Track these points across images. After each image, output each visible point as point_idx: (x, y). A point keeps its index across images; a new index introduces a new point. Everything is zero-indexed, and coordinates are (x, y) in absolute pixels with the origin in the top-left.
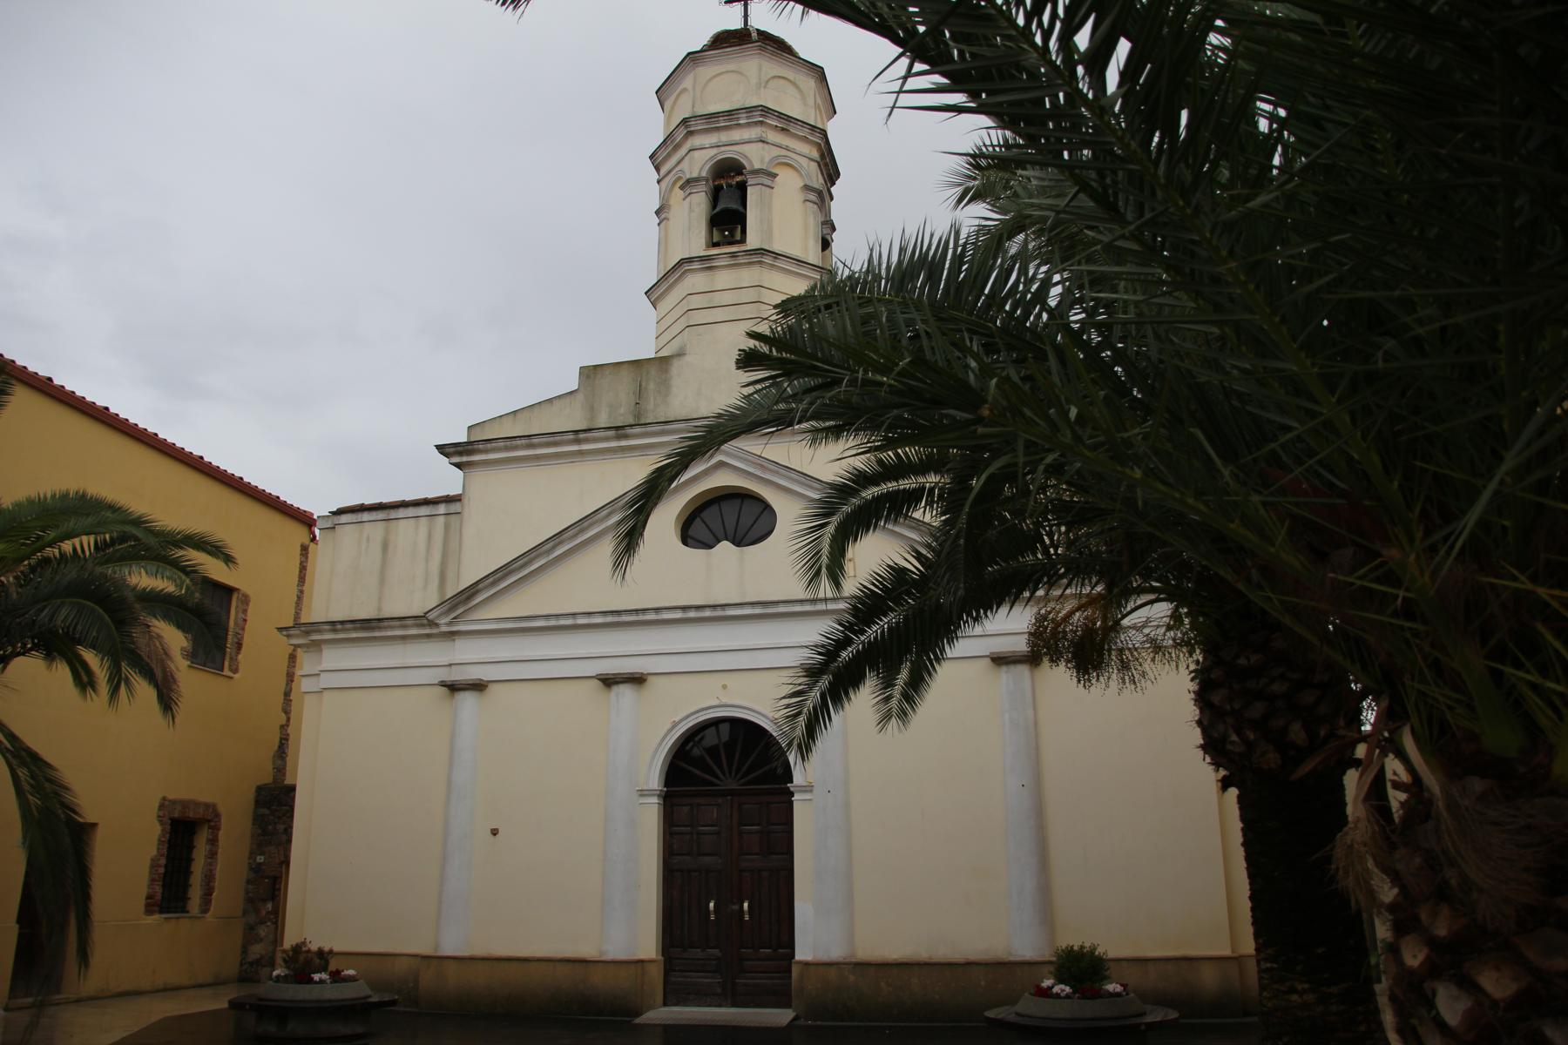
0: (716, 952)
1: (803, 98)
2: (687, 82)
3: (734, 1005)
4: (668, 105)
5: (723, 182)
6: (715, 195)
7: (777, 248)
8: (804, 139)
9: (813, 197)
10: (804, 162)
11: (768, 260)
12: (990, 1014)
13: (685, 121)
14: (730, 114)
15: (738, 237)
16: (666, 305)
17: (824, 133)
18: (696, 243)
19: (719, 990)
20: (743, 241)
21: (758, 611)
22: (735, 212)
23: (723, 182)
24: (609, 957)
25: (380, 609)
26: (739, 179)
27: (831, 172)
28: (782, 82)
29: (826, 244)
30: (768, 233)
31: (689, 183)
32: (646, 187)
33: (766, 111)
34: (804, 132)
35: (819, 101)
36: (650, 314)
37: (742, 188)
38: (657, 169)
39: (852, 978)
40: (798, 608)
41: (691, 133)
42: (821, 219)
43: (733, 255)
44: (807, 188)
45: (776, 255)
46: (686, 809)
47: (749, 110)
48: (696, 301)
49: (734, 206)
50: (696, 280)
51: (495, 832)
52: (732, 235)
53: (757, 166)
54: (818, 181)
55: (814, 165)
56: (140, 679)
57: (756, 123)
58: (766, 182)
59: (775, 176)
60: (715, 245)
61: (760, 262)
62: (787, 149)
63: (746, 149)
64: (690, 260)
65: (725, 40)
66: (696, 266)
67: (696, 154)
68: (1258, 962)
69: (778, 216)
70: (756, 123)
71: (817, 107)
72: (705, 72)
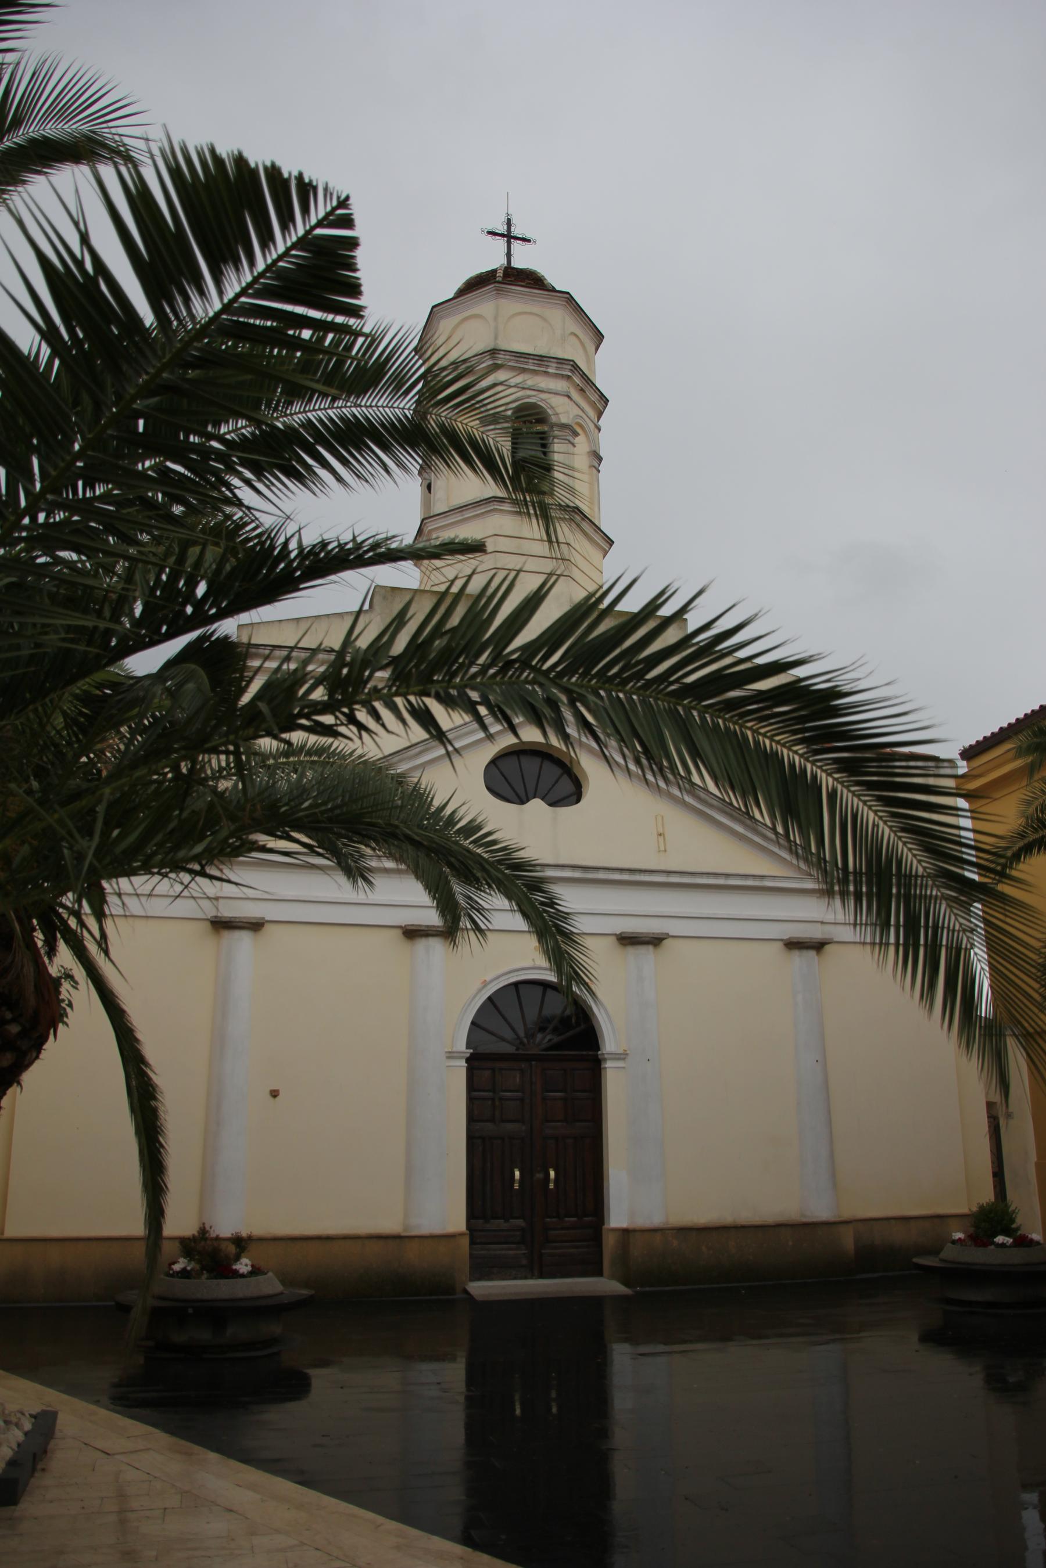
0: (520, 1222)
3: (542, 1276)
12: (915, 1260)
14: (541, 359)
19: (524, 1262)
21: (577, 874)
24: (425, 1231)
34: (594, 397)
39: (675, 1243)
40: (617, 876)
46: (487, 1073)
47: (561, 361)
51: (274, 1094)
53: (564, 420)
68: (472, 1243)
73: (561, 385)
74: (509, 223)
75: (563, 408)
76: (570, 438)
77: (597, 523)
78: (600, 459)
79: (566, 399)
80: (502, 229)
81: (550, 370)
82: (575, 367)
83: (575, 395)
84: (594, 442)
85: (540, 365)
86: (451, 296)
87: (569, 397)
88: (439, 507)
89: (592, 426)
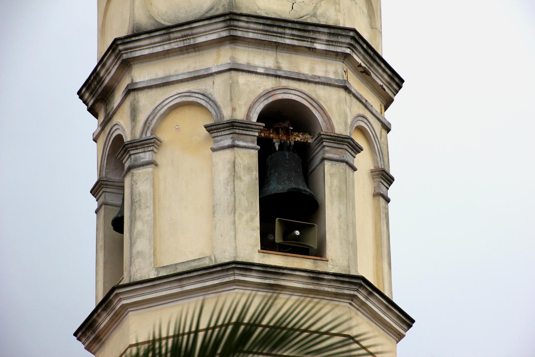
41: (233, 40)
47: (335, 31)
53: (340, 129)
57: (337, 55)
61: (352, 297)
63: (322, 93)
73: (332, 69)
75: (337, 111)
76: (348, 157)
77: (387, 294)
78: (389, 180)
79: (342, 93)
81: (318, 46)
82: (357, 39)
83: (356, 84)
84: (380, 153)
85: (301, 38)
87: (347, 89)
88: (141, 268)
89: (377, 126)
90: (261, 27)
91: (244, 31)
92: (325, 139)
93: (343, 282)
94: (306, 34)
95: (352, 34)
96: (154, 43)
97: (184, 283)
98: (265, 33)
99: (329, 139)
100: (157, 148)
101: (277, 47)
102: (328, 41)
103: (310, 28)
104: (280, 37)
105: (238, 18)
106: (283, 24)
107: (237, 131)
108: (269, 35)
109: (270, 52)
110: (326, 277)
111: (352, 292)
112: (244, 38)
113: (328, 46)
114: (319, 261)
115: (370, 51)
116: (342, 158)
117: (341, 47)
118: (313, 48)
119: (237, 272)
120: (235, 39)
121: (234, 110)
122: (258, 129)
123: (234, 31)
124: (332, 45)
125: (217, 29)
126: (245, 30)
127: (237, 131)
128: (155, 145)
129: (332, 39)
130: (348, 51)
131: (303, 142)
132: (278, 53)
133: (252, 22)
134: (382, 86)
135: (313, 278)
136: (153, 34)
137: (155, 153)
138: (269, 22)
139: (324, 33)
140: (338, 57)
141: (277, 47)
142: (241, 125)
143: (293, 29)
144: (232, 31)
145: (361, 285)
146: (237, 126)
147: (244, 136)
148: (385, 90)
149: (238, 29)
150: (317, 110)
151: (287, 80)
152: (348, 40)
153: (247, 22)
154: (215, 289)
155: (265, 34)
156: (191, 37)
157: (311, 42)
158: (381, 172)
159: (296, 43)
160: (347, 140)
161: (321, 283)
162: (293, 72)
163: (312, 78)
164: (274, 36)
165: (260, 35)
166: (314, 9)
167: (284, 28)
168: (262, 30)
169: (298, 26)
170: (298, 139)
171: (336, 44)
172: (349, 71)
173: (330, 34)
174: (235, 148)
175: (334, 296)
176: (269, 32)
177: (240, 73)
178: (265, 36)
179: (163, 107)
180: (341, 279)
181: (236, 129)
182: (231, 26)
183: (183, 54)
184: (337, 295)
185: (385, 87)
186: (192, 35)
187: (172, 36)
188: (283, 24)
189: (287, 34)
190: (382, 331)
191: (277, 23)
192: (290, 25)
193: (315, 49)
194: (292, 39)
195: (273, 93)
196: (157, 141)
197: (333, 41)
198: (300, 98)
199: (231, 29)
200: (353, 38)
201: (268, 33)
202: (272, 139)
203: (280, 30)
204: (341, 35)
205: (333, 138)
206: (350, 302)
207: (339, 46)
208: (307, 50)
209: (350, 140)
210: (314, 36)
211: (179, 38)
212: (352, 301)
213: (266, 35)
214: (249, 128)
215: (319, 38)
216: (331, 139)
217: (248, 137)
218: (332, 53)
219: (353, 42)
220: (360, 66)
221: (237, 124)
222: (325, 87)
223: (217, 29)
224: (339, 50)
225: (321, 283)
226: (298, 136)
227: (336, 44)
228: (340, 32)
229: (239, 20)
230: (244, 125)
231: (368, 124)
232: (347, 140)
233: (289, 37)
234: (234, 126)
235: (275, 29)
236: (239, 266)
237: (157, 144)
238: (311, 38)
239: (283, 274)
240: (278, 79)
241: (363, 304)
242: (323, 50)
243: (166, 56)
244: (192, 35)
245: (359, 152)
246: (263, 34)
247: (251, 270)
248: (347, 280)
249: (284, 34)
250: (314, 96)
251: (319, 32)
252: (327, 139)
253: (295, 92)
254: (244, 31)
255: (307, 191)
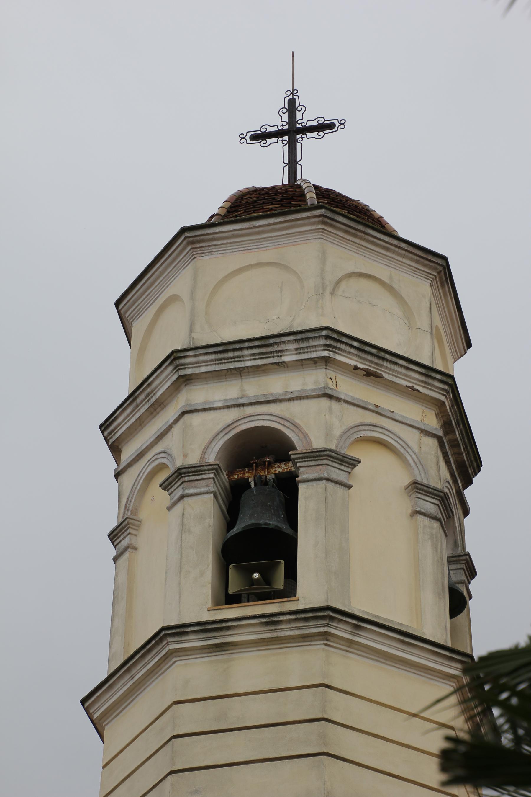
1: (408, 313)
2: (180, 282)
4: (139, 327)
5: (250, 476)
6: (233, 501)
7: (358, 607)
8: (411, 393)
9: (430, 506)
10: (411, 437)
11: (341, 631)
13: (174, 357)
14: (264, 343)
15: (280, 583)
16: (122, 728)
17: (449, 382)
18: (197, 602)
20: (290, 590)
22: (276, 532)
23: (250, 476)
25: (327, 601)
26: (281, 468)
27: (463, 457)
28: (364, 283)
29: (458, 603)
30: (340, 574)
31: (181, 476)
32: (94, 487)
33: (335, 338)
35: (438, 321)
36: (94, 748)
37: (288, 487)
38: (115, 449)
41: (186, 380)
42: (446, 552)
43: (270, 620)
44: (418, 488)
45: (359, 622)
47: (302, 336)
48: (191, 718)
49: (273, 521)
50: (191, 673)
52: (267, 579)
53: (318, 443)
54: (439, 475)
55: (431, 444)
56: (439, 487)
57: (315, 361)
58: (341, 476)
59: (352, 463)
60: (231, 599)
61: (325, 636)
62: (377, 411)
63: (295, 410)
64: (179, 630)
65: (249, 207)
66: (192, 642)
67: (195, 420)
69: (358, 542)
70: (315, 361)
71: (435, 334)
72: (214, 265)
73: (313, 379)
74: (260, 137)
79: (325, 402)
80: (278, 149)
85: (264, 355)
86: (203, 220)
90: (213, 357)
91: (194, 367)
92: (297, 459)
93: (306, 619)
94: (269, 349)
95: (324, 333)
96: (128, 416)
97: (133, 672)
98: (220, 362)
99: (302, 458)
100: (137, 530)
101: (240, 374)
102: (297, 349)
103: (272, 341)
104: (238, 361)
105: (182, 354)
106: (238, 346)
107: (187, 479)
108: (225, 363)
109: (234, 382)
110: (282, 618)
111: (322, 630)
112: (197, 374)
113: (300, 355)
114: (286, 603)
115: (367, 349)
116: (321, 475)
117: (316, 351)
118: (281, 362)
119: (170, 639)
120: (188, 380)
121: (185, 456)
122: (212, 470)
123: (183, 371)
124: (305, 353)
125: (169, 375)
126: (195, 365)
127: (187, 479)
128: (131, 526)
129: (302, 345)
130: (326, 353)
131: (287, 472)
132: (244, 380)
133: (200, 355)
134: (413, 388)
135: (267, 624)
136: (124, 407)
137: (136, 535)
138: (221, 348)
139: (289, 341)
140: (318, 364)
141: (240, 374)
142: (190, 470)
143: (251, 348)
144: (180, 371)
145: (332, 619)
146: (185, 473)
147: (196, 482)
148: (419, 391)
149: (186, 366)
150: (291, 429)
151: (253, 406)
152: (322, 341)
153: (195, 356)
154: (160, 670)
155: (221, 363)
156: (152, 394)
157: (278, 356)
158: (414, 485)
159: (259, 362)
160: (325, 453)
161: (279, 627)
162: (259, 396)
163: (283, 396)
164: (231, 362)
165: (214, 366)
166: (291, 322)
167: (241, 349)
168: (216, 360)
169: (256, 343)
170: (279, 470)
171: (309, 350)
172: (339, 377)
173: (298, 341)
174: (185, 498)
175: (301, 639)
176: (224, 359)
177: (195, 415)
178: (221, 366)
179: (139, 482)
180: (303, 616)
181: (185, 477)
182: (177, 366)
183: (155, 416)
184: (305, 638)
185: (416, 387)
186: (152, 391)
187: (139, 400)
188: (238, 346)
189: (247, 356)
190: (413, 675)
191: (231, 347)
192: (247, 344)
193: (284, 362)
194: (254, 359)
195: (235, 425)
196: (132, 521)
197: (303, 348)
198: (270, 422)
199: (179, 369)
200: (327, 337)
201: (223, 361)
202: (248, 479)
203: (237, 354)
204: (312, 338)
205: (306, 455)
206: (325, 642)
207: (313, 351)
208: (276, 367)
209: (328, 452)
210: (279, 349)
211: (144, 400)
212: (327, 640)
213: (222, 363)
214: (199, 471)
215: (285, 348)
216: (304, 458)
217: (201, 482)
218: (308, 362)
219: (328, 342)
220: (356, 368)
221: (184, 471)
222: (302, 401)
223: (169, 375)
224: (314, 355)
225: (279, 627)
226: (279, 467)
227: (309, 350)
228: (309, 335)
229: (185, 357)
230: (193, 469)
231: (387, 433)
232: (325, 453)
233: (249, 358)
234: (181, 474)
235: (230, 354)
236: (170, 632)
237: (133, 524)
238: (276, 351)
239: (228, 628)
240: (242, 408)
241: (351, 643)
242: (293, 361)
243: (143, 425)
244: (152, 391)
245: (355, 466)
246: (218, 364)
247: (187, 633)
248: (310, 615)
249: (243, 356)
250: (287, 415)
251: (284, 342)
252: (299, 458)
253: (262, 418)
254: (194, 367)
255: (270, 524)
